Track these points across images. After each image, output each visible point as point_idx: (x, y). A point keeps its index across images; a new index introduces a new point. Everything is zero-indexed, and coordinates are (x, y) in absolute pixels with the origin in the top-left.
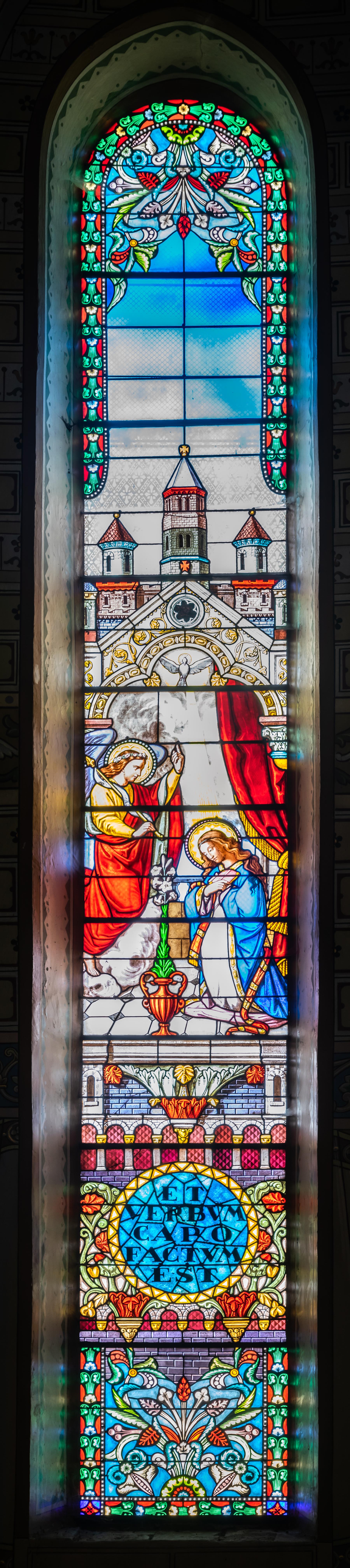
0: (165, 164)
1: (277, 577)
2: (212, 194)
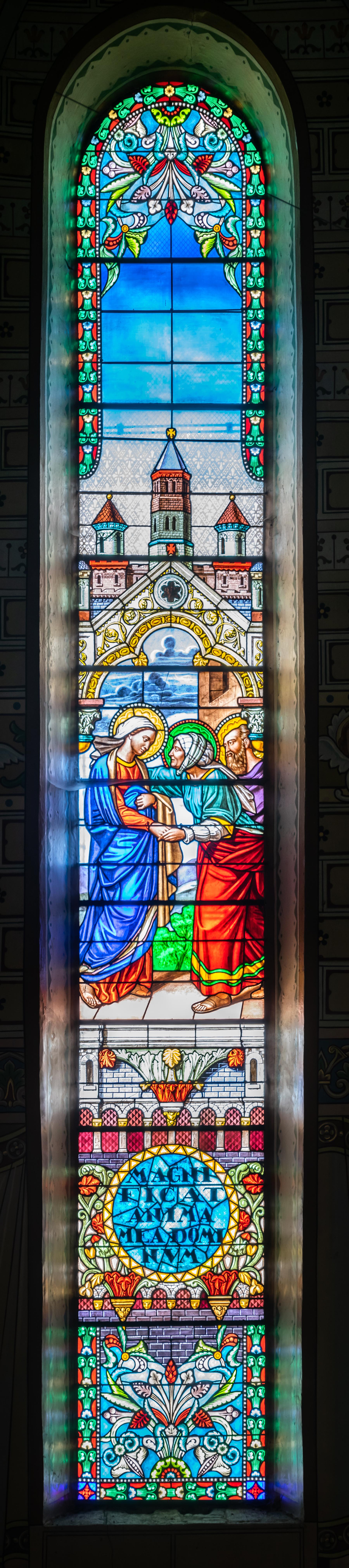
0: (154, 147)
1: (254, 560)
2: (197, 178)
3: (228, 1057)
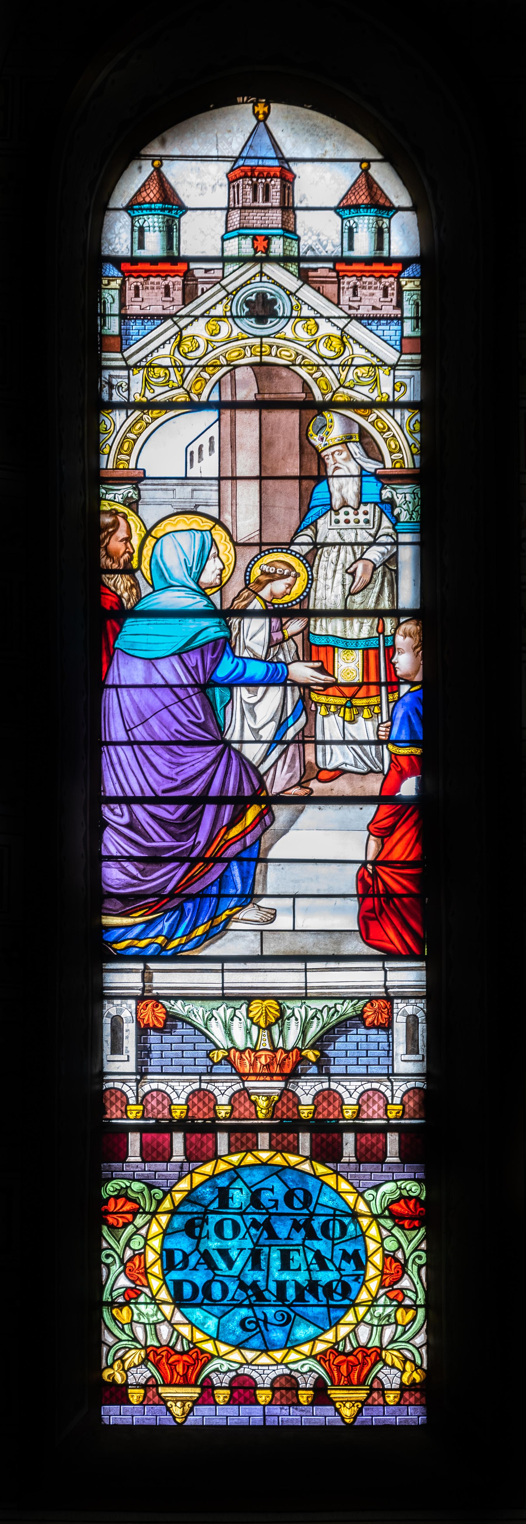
3: (363, 1012)
